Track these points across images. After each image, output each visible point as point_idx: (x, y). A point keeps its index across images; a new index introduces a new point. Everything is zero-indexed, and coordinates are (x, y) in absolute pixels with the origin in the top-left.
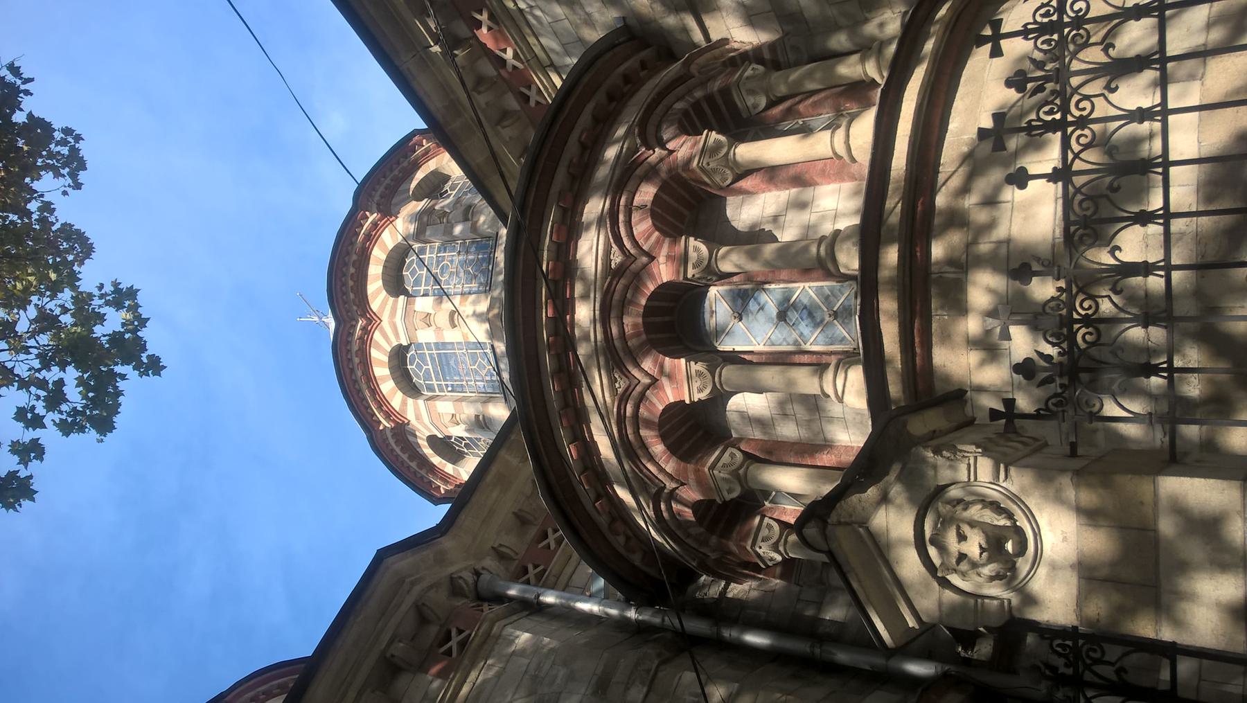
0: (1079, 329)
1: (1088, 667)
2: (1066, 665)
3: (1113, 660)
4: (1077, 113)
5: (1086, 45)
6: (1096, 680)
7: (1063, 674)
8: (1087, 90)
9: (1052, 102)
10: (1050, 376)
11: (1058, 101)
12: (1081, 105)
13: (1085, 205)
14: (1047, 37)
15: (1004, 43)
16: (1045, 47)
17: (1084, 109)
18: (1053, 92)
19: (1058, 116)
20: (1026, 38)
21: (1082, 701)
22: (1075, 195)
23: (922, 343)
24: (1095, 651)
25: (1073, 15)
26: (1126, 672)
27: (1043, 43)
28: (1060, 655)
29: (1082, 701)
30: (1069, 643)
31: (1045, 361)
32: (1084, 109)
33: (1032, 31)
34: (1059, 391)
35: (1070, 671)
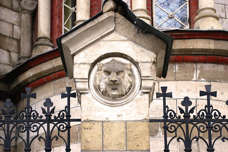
0: (25, 124)
1: (55, 125)
2: (55, 117)
3: (60, 135)
4: (169, 126)
5: (199, 130)
6: (51, 129)
7: (51, 115)
8: (179, 129)
9: (175, 116)
10: (184, 112)
11: (220, 118)
12: (172, 127)
13: (217, 127)
14: (205, 115)
15: (205, 97)
16: (201, 113)
17: (171, 129)
18: (180, 117)
19: (169, 118)
20: (206, 106)
21: (1, 123)
22: (222, 124)
23: (180, 33)
24: (63, 128)
25: (213, 126)
26: (56, 140)
27: (203, 113)
28: (59, 114)
29: (1, 123)
30: (65, 118)
31: (51, 111)
32: (171, 129)
33: (209, 110)
34: (39, 115)
35: (52, 118)
